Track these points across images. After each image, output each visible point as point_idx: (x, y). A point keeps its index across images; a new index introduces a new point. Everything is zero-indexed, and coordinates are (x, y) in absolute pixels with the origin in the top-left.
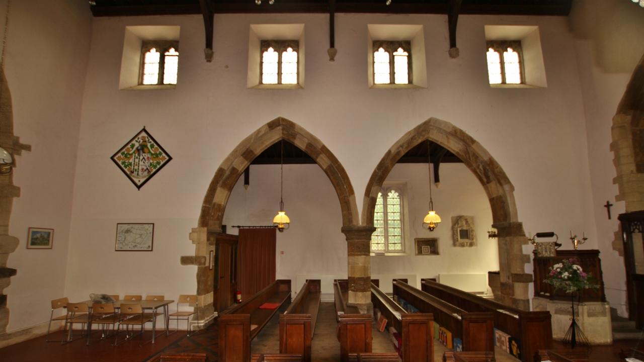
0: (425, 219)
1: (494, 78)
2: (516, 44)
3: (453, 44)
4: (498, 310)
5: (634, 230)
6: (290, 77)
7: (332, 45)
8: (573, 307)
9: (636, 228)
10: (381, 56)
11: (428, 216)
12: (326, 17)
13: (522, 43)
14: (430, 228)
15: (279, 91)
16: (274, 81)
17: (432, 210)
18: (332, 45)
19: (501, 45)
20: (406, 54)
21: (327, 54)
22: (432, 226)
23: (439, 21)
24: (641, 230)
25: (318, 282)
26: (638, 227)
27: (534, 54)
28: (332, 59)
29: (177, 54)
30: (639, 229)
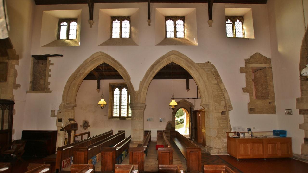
0: (99, 103)
1: (230, 34)
2: (241, 18)
3: (210, 18)
4: (113, 147)
5: (6, 108)
6: (126, 34)
7: (149, 18)
8: (218, 150)
9: (7, 107)
10: (116, 24)
11: (100, 101)
12: (146, 4)
13: (244, 17)
14: (101, 107)
15: (174, 41)
16: (118, 36)
17: (103, 99)
18: (149, 18)
19: (233, 19)
20: (129, 22)
21: (147, 22)
22: (102, 106)
23: (204, 6)
24: (2, 108)
25: (60, 130)
26: (8, 107)
27: (250, 21)
28: (149, 25)
29: (231, 22)
30: (8, 108)
